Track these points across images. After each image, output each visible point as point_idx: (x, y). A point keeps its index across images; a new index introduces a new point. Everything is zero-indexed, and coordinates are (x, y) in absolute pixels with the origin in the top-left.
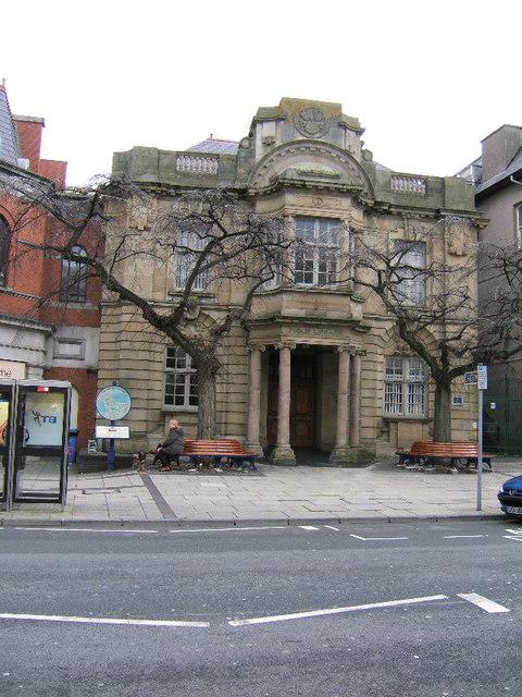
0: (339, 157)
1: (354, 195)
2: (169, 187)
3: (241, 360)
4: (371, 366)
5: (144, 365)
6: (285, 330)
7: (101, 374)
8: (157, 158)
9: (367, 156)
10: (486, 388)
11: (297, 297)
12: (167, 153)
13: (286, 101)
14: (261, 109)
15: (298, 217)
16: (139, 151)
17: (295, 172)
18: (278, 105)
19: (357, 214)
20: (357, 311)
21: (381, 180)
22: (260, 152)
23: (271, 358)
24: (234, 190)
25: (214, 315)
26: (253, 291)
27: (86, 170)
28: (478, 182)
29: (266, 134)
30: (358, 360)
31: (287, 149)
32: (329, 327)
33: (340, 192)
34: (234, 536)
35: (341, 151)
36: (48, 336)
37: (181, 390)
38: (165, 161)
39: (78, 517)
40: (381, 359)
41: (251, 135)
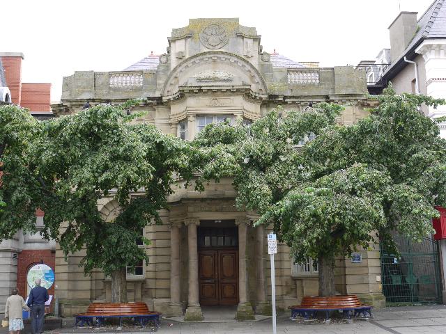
10: (276, 252)
12: (102, 74)
15: (198, 116)
16: (78, 75)
22: (174, 63)
29: (178, 50)
31: (193, 60)
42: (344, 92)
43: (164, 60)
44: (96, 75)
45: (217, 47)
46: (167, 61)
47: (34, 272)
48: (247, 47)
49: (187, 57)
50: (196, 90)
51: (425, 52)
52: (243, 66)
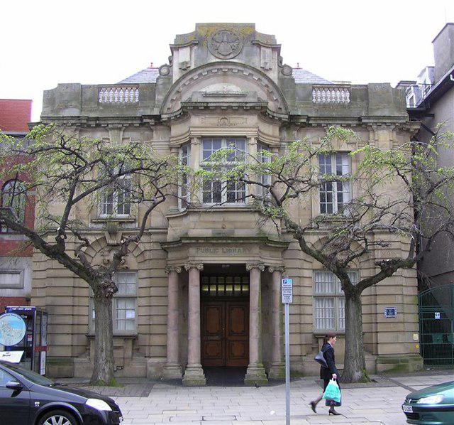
0: (252, 75)
1: (261, 111)
3: (158, 282)
5: (69, 292)
6: (192, 251)
8: (84, 95)
9: (286, 71)
18: (194, 30)
19: (270, 132)
22: (176, 75)
23: (183, 278)
24: (150, 117)
27: (394, 86)
28: (433, 84)
30: (44, 317)
31: (199, 72)
32: (237, 245)
33: (243, 109)
35: (253, 69)
38: (88, 94)
44: (83, 88)
45: (228, 57)
46: (169, 71)
52: (259, 79)
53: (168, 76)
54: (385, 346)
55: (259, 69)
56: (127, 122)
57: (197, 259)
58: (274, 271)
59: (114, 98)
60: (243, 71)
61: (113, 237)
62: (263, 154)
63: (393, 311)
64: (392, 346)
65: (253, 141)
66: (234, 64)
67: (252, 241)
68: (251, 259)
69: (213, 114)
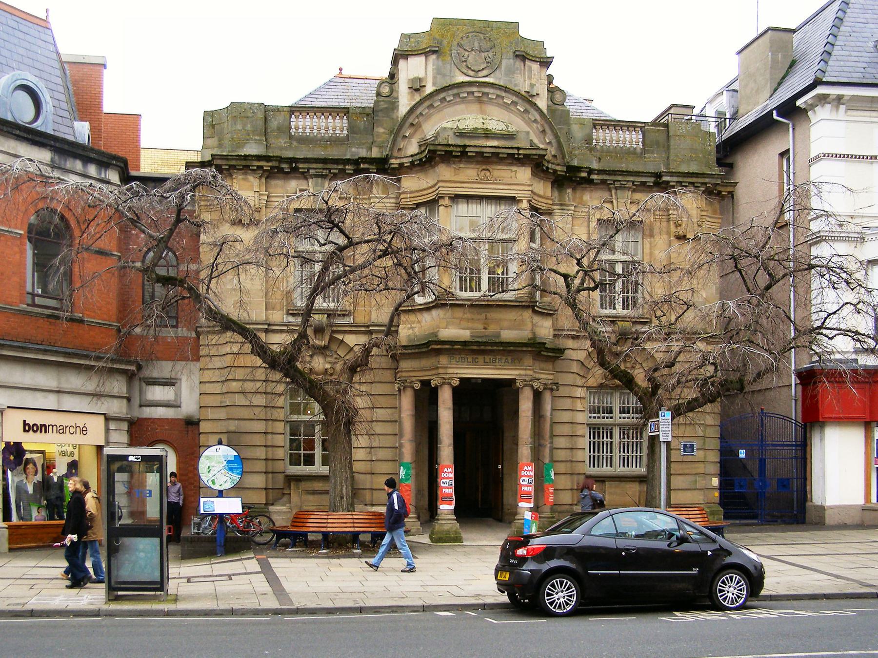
2: (281, 159)
4: (567, 404)
6: (444, 360)
7: (204, 427)
9: (558, 97)
11: (459, 313)
12: (277, 109)
13: (443, 25)
14: (406, 37)
16: (237, 111)
17: (451, 133)
19: (543, 188)
20: (544, 329)
21: (578, 133)
22: (405, 101)
25: (351, 340)
26: (400, 305)
28: (734, 117)
30: (547, 397)
31: (442, 95)
33: (516, 159)
34: (330, 623)
35: (517, 94)
36: (130, 377)
37: (310, 445)
39: (181, 606)
40: (580, 392)
41: (392, 76)
42: (684, 169)
43: (386, 90)
44: (268, 111)
45: (481, 74)
46: (392, 91)
47: (208, 458)
48: (530, 78)
49: (429, 89)
50: (457, 151)
51: (812, 107)
52: (526, 111)
53: (392, 101)
54: (680, 493)
55: (523, 93)
56: (335, 166)
57: (450, 371)
58: (545, 389)
59: (312, 129)
60: (503, 98)
61: (319, 336)
62: (214, 177)
63: (692, 446)
64: (689, 493)
65: (525, 204)
66: (492, 85)
67: (525, 349)
68: (522, 372)
69: (472, 163)
